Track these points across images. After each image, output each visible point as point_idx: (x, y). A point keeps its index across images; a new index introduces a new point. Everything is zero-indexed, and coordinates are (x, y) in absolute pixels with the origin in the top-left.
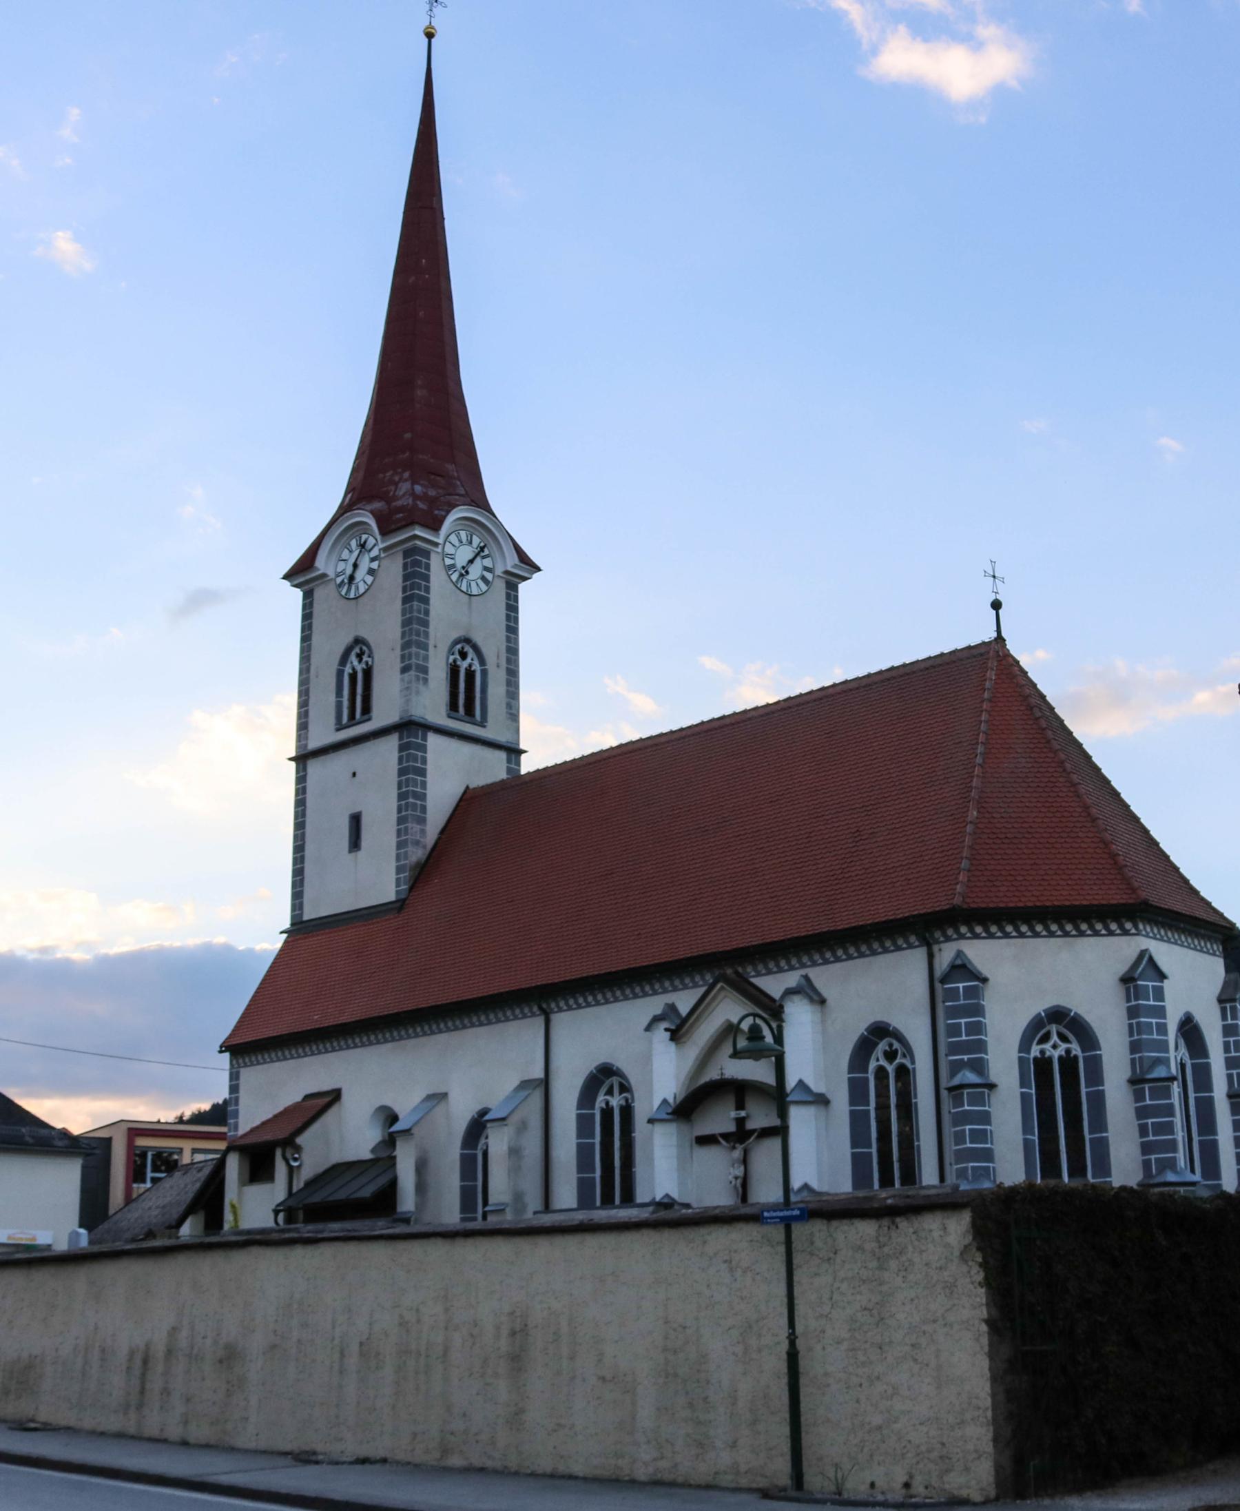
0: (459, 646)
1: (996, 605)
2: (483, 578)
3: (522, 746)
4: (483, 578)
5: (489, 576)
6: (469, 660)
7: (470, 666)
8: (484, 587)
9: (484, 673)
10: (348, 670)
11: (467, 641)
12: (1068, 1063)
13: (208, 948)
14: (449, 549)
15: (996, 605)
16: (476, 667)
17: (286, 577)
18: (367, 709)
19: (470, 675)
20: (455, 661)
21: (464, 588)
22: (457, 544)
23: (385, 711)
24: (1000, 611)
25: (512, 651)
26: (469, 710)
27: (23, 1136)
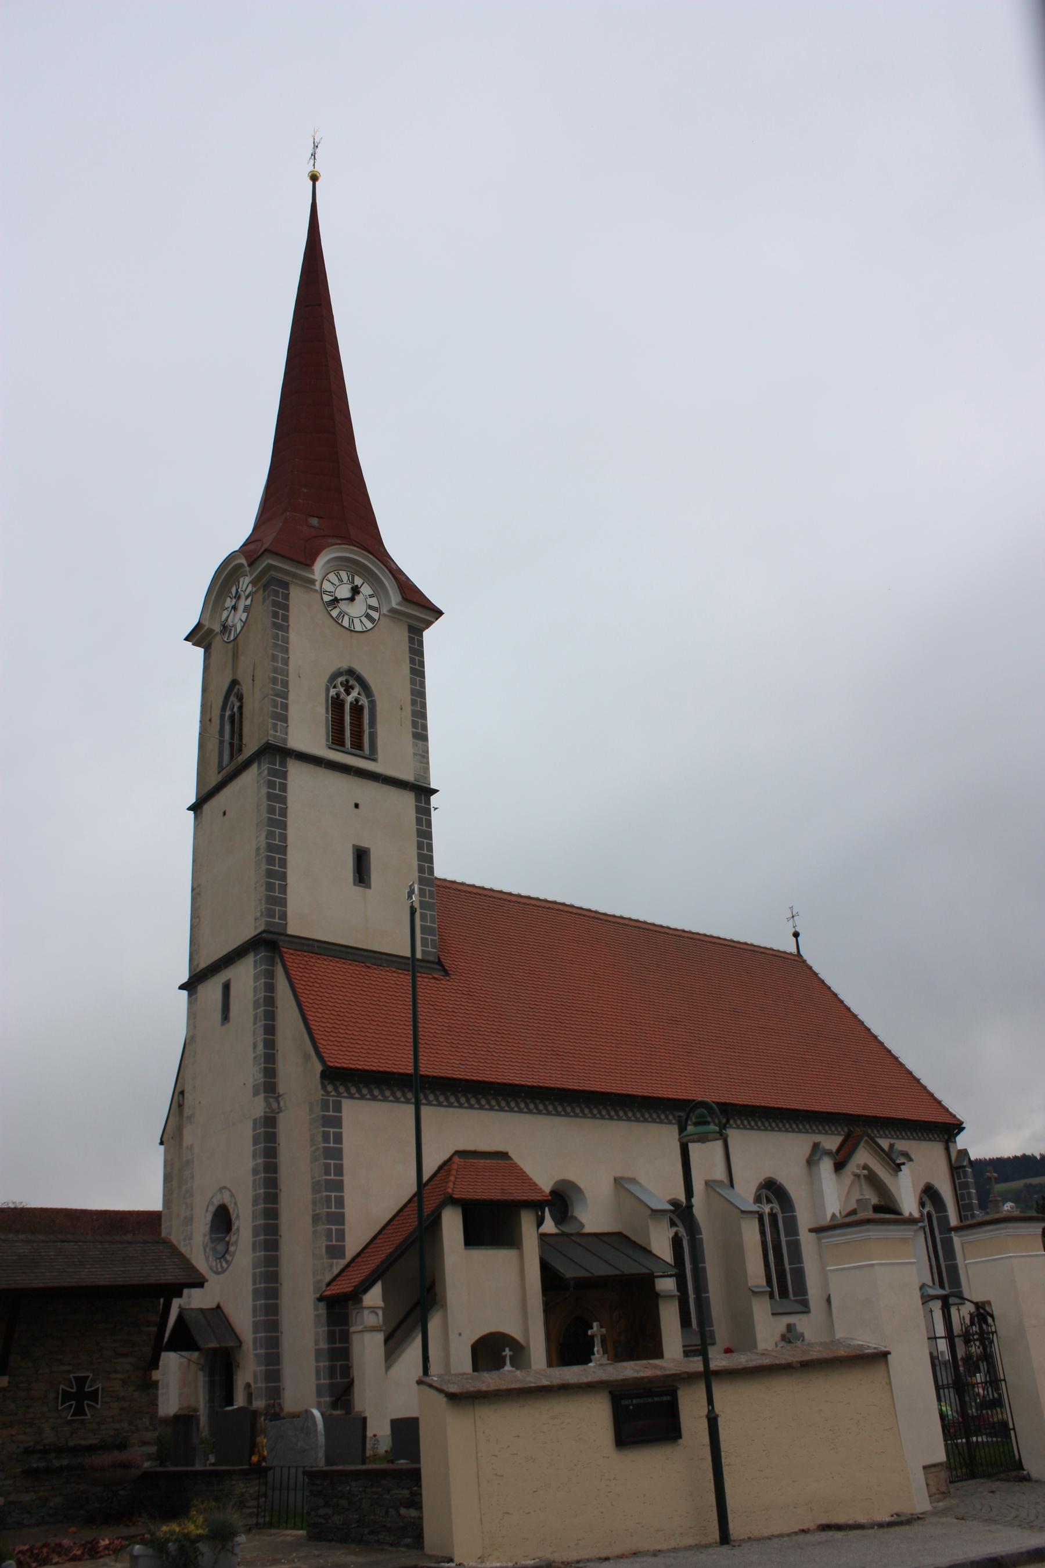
0: (340, 679)
1: (314, 178)
2: (368, 616)
3: (433, 785)
4: (368, 616)
5: (375, 615)
6: (354, 694)
7: (357, 700)
8: (369, 625)
9: (373, 704)
10: (228, 713)
11: (351, 672)
12: (357, 709)
13: (1024, 1156)
14: (327, 586)
15: (314, 178)
16: (364, 701)
17: (186, 639)
18: (240, 750)
19: (357, 709)
20: (338, 695)
21: (346, 623)
22: (336, 582)
23: (251, 745)
24: (317, 183)
25: (418, 694)
26: (357, 744)
27: (592, 1328)
